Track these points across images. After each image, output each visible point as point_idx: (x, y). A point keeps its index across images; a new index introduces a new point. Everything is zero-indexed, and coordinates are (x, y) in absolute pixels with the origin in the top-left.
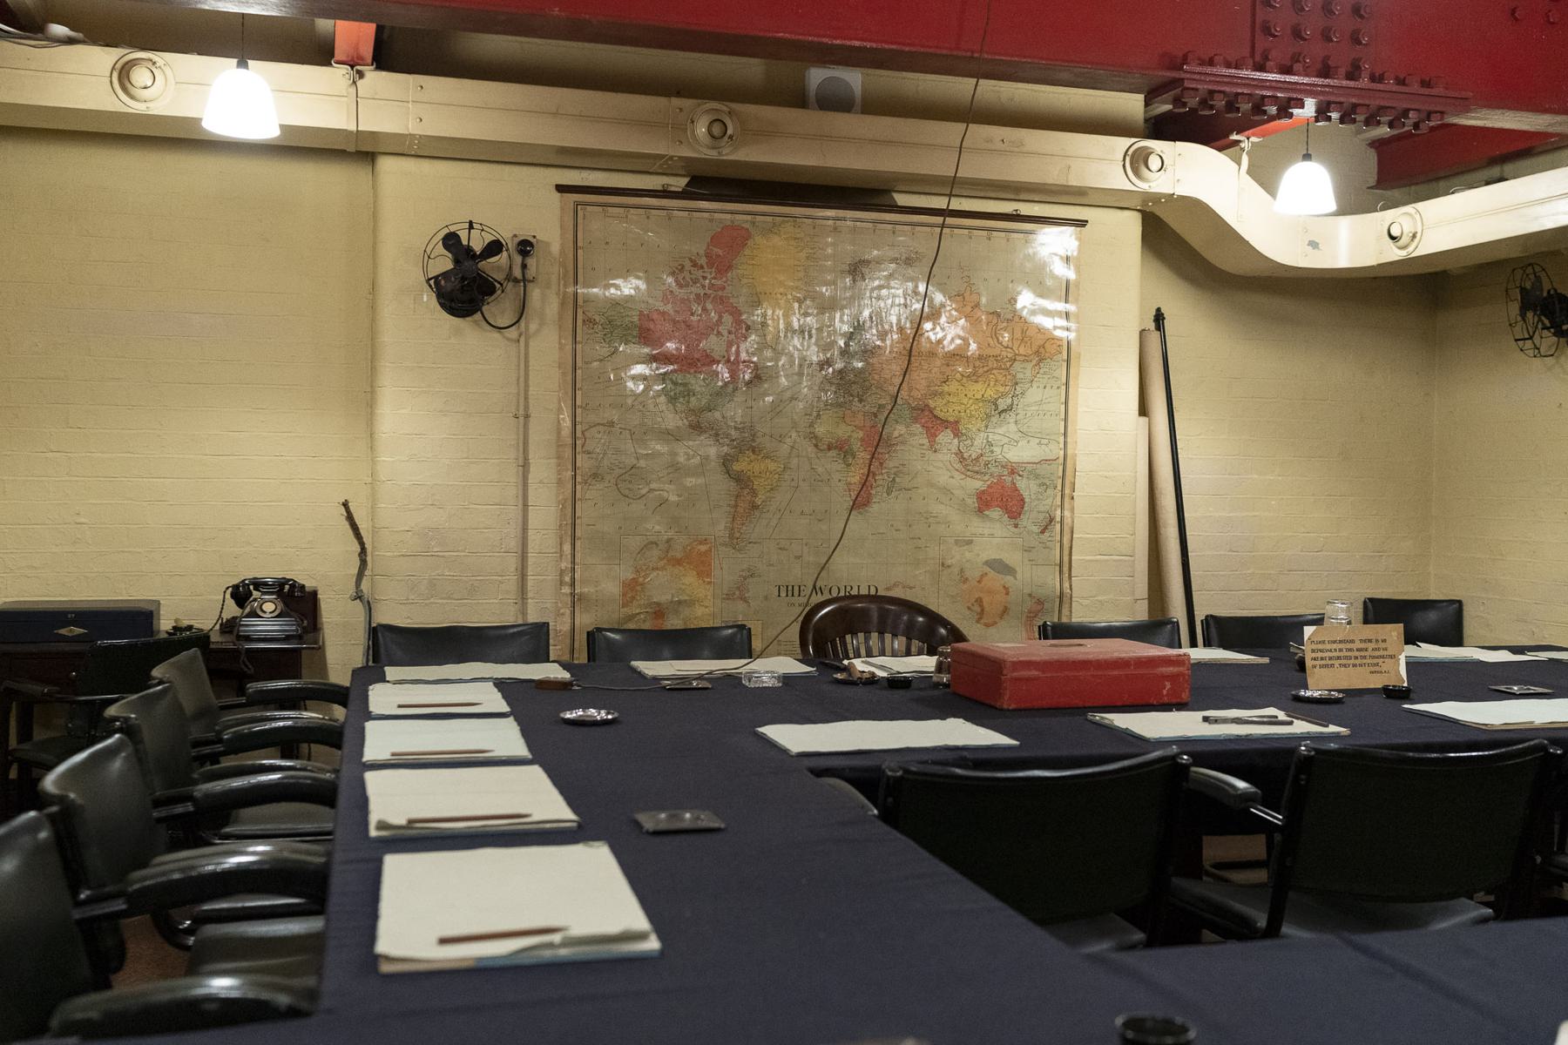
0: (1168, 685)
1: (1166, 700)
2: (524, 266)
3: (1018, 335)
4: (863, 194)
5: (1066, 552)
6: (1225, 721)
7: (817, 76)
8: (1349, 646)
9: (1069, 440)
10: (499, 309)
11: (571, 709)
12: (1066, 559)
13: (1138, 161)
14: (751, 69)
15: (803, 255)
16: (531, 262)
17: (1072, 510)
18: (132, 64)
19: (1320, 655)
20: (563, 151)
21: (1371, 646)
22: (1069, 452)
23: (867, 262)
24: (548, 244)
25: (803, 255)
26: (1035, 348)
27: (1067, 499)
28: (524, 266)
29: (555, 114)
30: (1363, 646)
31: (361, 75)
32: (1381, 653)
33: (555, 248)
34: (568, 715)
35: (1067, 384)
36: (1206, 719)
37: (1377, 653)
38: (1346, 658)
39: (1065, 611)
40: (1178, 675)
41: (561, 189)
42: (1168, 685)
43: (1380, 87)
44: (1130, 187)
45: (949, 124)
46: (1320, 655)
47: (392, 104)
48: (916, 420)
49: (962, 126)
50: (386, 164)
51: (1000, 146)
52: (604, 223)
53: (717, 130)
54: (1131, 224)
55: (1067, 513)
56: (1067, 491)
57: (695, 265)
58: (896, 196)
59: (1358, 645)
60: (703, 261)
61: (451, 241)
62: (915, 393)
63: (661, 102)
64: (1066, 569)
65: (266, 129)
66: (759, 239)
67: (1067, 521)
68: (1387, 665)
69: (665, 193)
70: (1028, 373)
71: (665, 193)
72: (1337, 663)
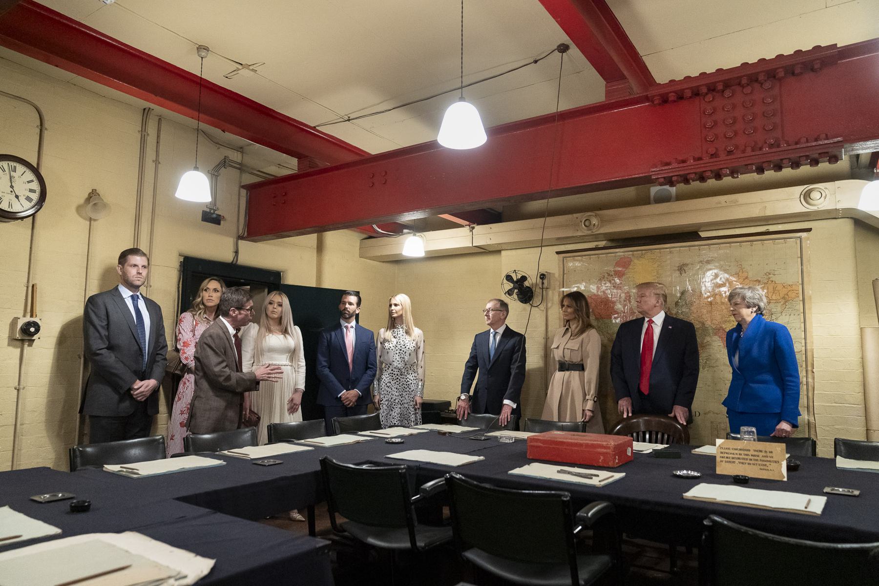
0: (602, 458)
1: (601, 464)
2: (543, 283)
3: (771, 289)
4: (689, 235)
5: (811, 401)
6: (569, 473)
7: (654, 190)
8: (746, 452)
9: (808, 341)
10: (536, 300)
11: (681, 469)
12: (811, 404)
13: (807, 196)
14: (629, 192)
15: (656, 265)
16: (545, 281)
17: (813, 378)
18: (810, 191)
19: (726, 455)
20: (558, 239)
21: (761, 454)
22: (808, 348)
23: (686, 265)
24: (554, 274)
25: (656, 265)
26: (782, 296)
27: (810, 373)
28: (543, 283)
29: (567, 226)
30: (756, 453)
31: (473, 228)
32: (769, 459)
33: (557, 275)
34: (678, 473)
35: (804, 313)
36: (559, 472)
37: (765, 459)
38: (744, 459)
39: (812, 432)
40: (606, 453)
41: (558, 253)
42: (602, 458)
43: (732, 157)
44: (804, 210)
45: (702, 200)
46: (726, 455)
47: (485, 235)
48: (716, 334)
49: (543, 219)
50: (503, 252)
51: (724, 204)
52: (573, 264)
53: (587, 223)
54: (846, 227)
55: (810, 380)
56: (809, 368)
57: (609, 275)
58: (700, 233)
59: (752, 452)
60: (613, 273)
61: (509, 278)
62: (714, 322)
63: (570, 216)
64: (811, 410)
65: (421, 254)
66: (636, 261)
67: (810, 384)
68: (773, 466)
69: (597, 248)
70: (779, 309)
71: (597, 248)
72: (737, 461)
